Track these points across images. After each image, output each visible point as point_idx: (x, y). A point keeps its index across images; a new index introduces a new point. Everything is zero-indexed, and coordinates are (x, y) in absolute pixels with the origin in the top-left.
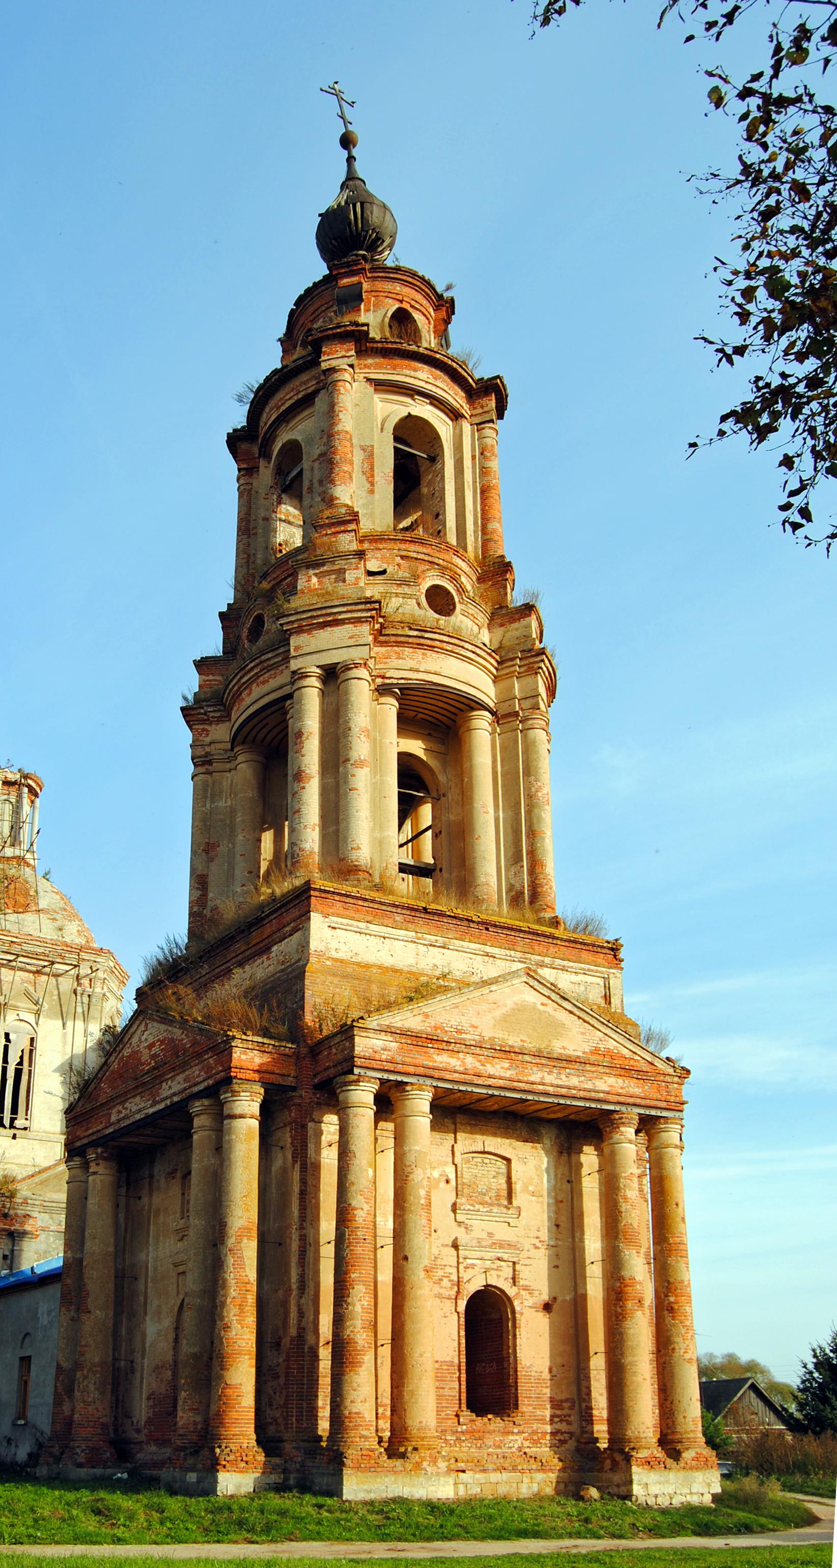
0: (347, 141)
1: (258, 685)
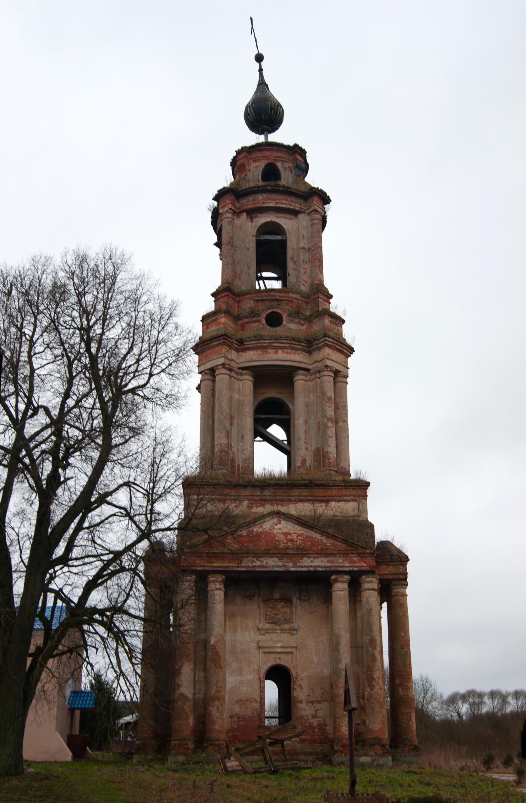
0: (259, 58)
1: (283, 352)
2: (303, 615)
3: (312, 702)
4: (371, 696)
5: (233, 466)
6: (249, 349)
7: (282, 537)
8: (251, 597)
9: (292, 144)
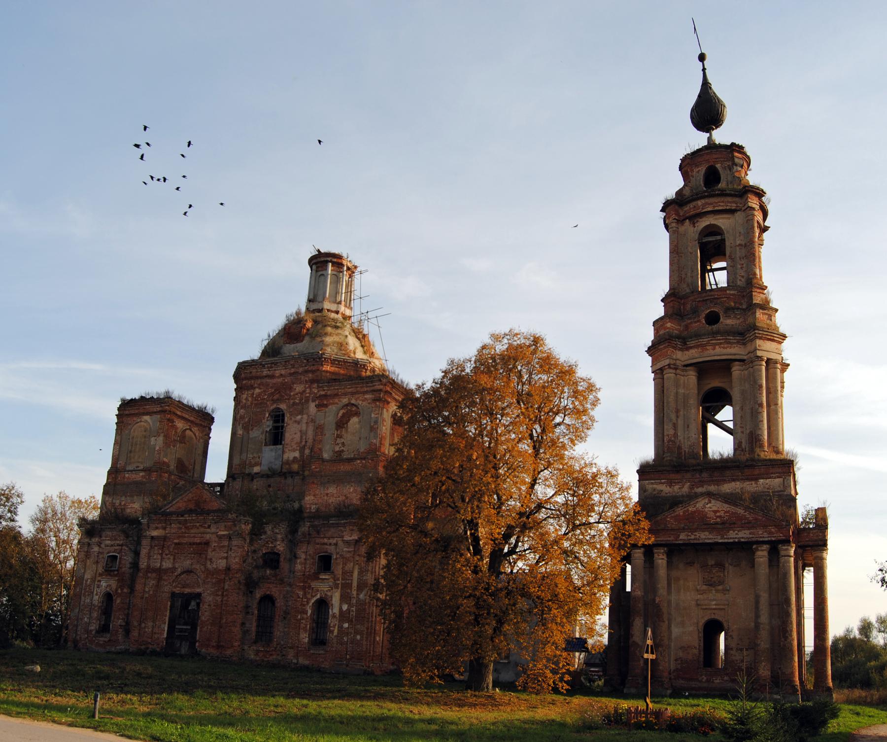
0: (702, 58)
2: (734, 579)
3: (741, 650)
4: (785, 645)
5: (679, 453)
6: (691, 348)
7: (712, 514)
8: (691, 564)
9: (729, 144)
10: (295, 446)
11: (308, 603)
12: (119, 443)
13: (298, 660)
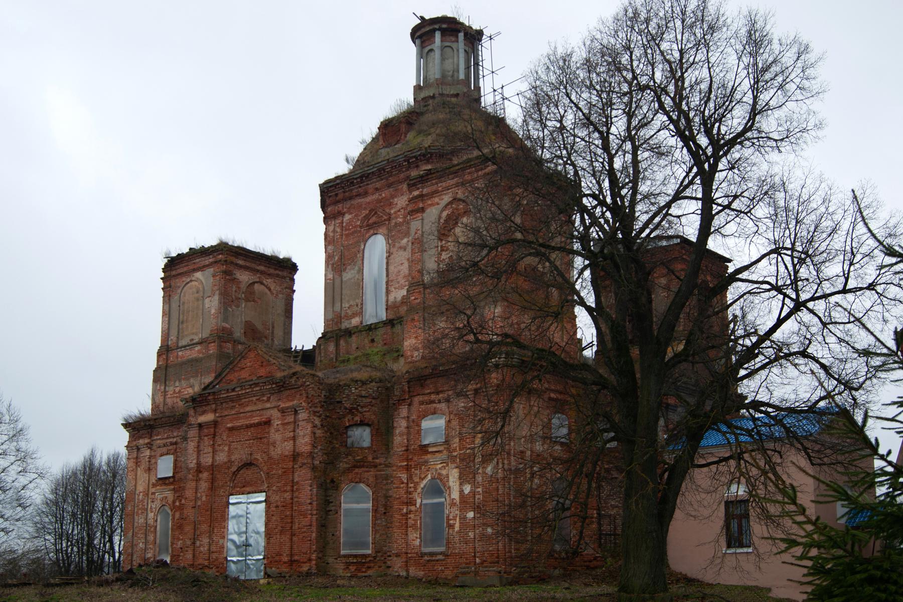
10: (402, 282)
11: (416, 489)
12: (167, 314)
13: (407, 571)
